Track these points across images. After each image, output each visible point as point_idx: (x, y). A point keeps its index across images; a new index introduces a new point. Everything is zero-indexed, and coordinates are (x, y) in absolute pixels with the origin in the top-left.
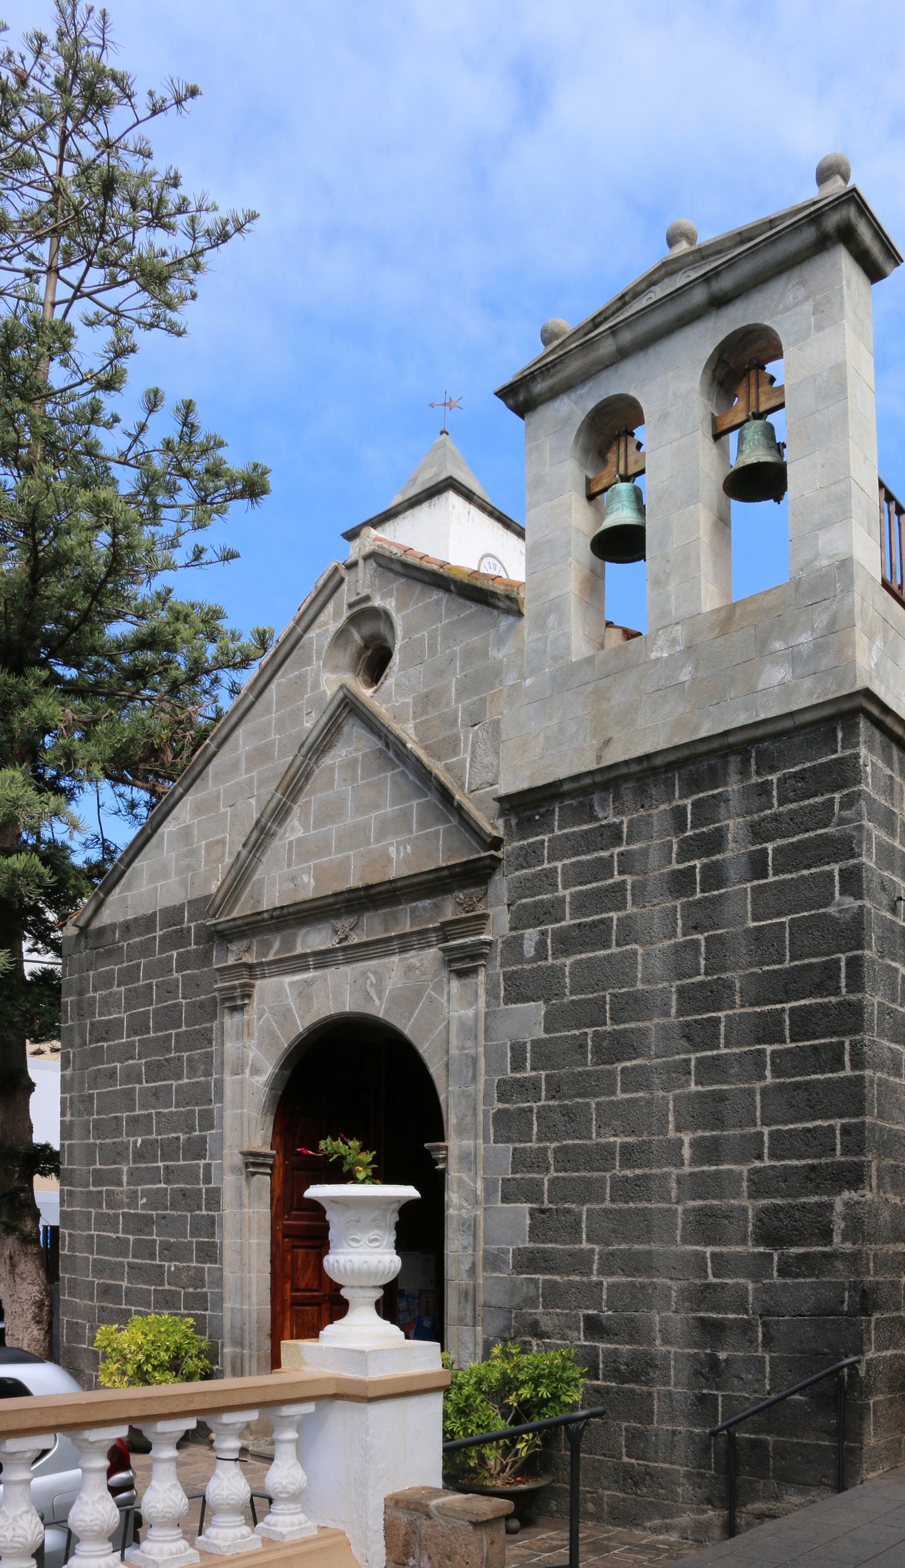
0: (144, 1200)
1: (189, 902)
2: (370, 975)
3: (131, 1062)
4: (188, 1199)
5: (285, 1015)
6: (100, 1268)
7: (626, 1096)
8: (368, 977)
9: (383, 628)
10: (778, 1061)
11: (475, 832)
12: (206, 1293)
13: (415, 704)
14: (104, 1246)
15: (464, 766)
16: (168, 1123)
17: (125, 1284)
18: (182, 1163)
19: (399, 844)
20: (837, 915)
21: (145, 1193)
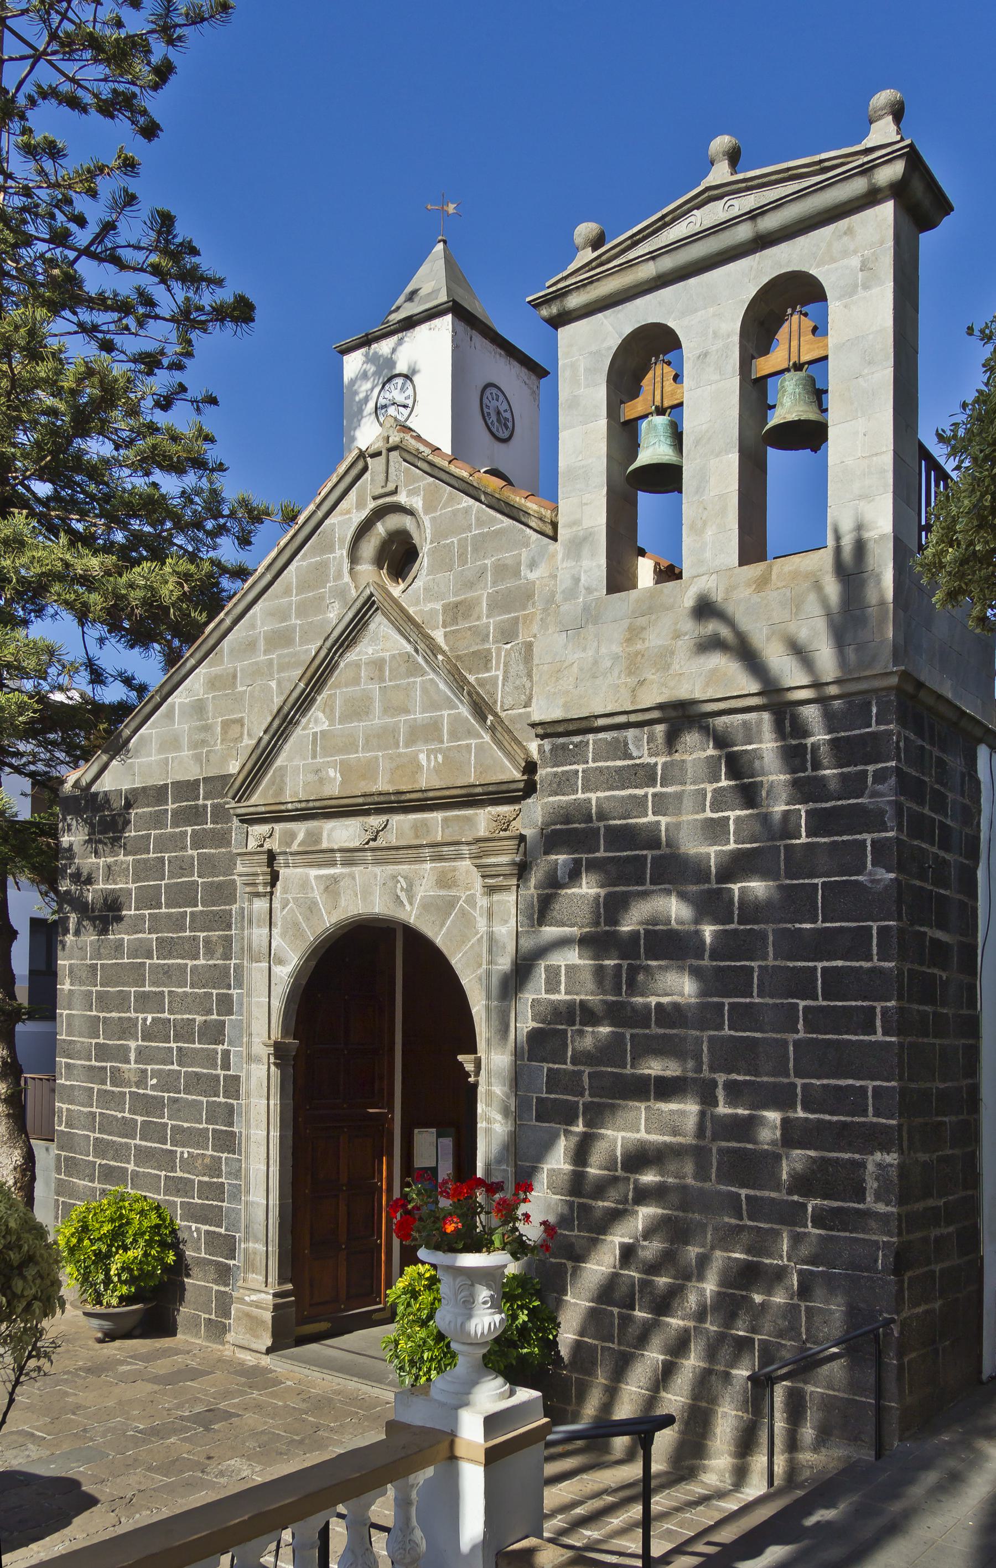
0: (154, 1081)
1: (204, 779)
2: (399, 878)
3: (140, 935)
4: (206, 1084)
5: (311, 908)
6: (101, 1148)
7: (661, 1031)
8: (398, 881)
9: (407, 522)
10: (810, 1016)
11: (880, 1379)
12: (223, 1184)
13: (444, 612)
14: (107, 1125)
15: (496, 684)
16: (180, 1003)
17: (131, 1167)
18: (197, 1045)
19: (429, 752)
20: (869, 885)
21: (155, 1074)
